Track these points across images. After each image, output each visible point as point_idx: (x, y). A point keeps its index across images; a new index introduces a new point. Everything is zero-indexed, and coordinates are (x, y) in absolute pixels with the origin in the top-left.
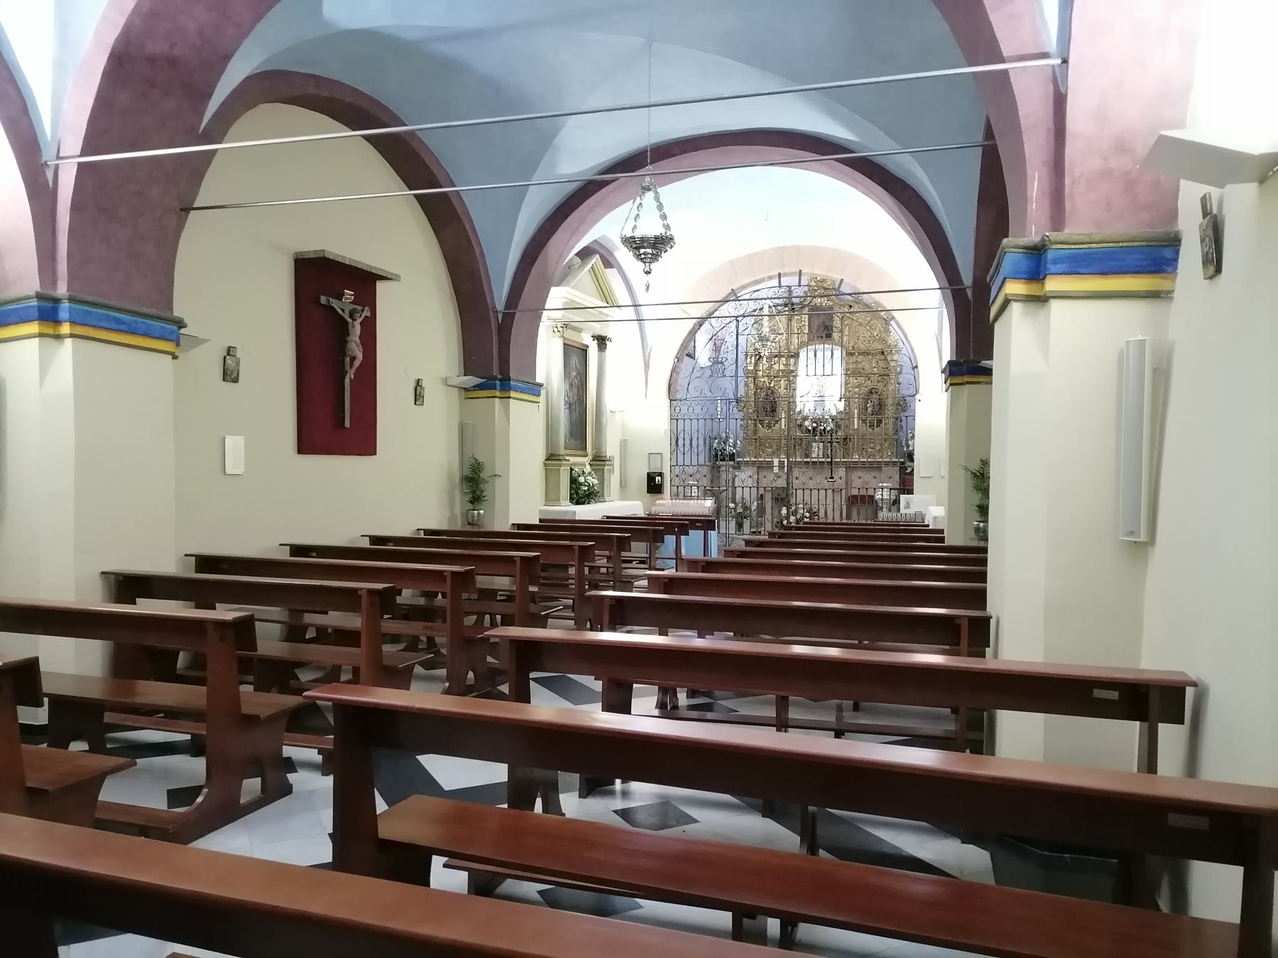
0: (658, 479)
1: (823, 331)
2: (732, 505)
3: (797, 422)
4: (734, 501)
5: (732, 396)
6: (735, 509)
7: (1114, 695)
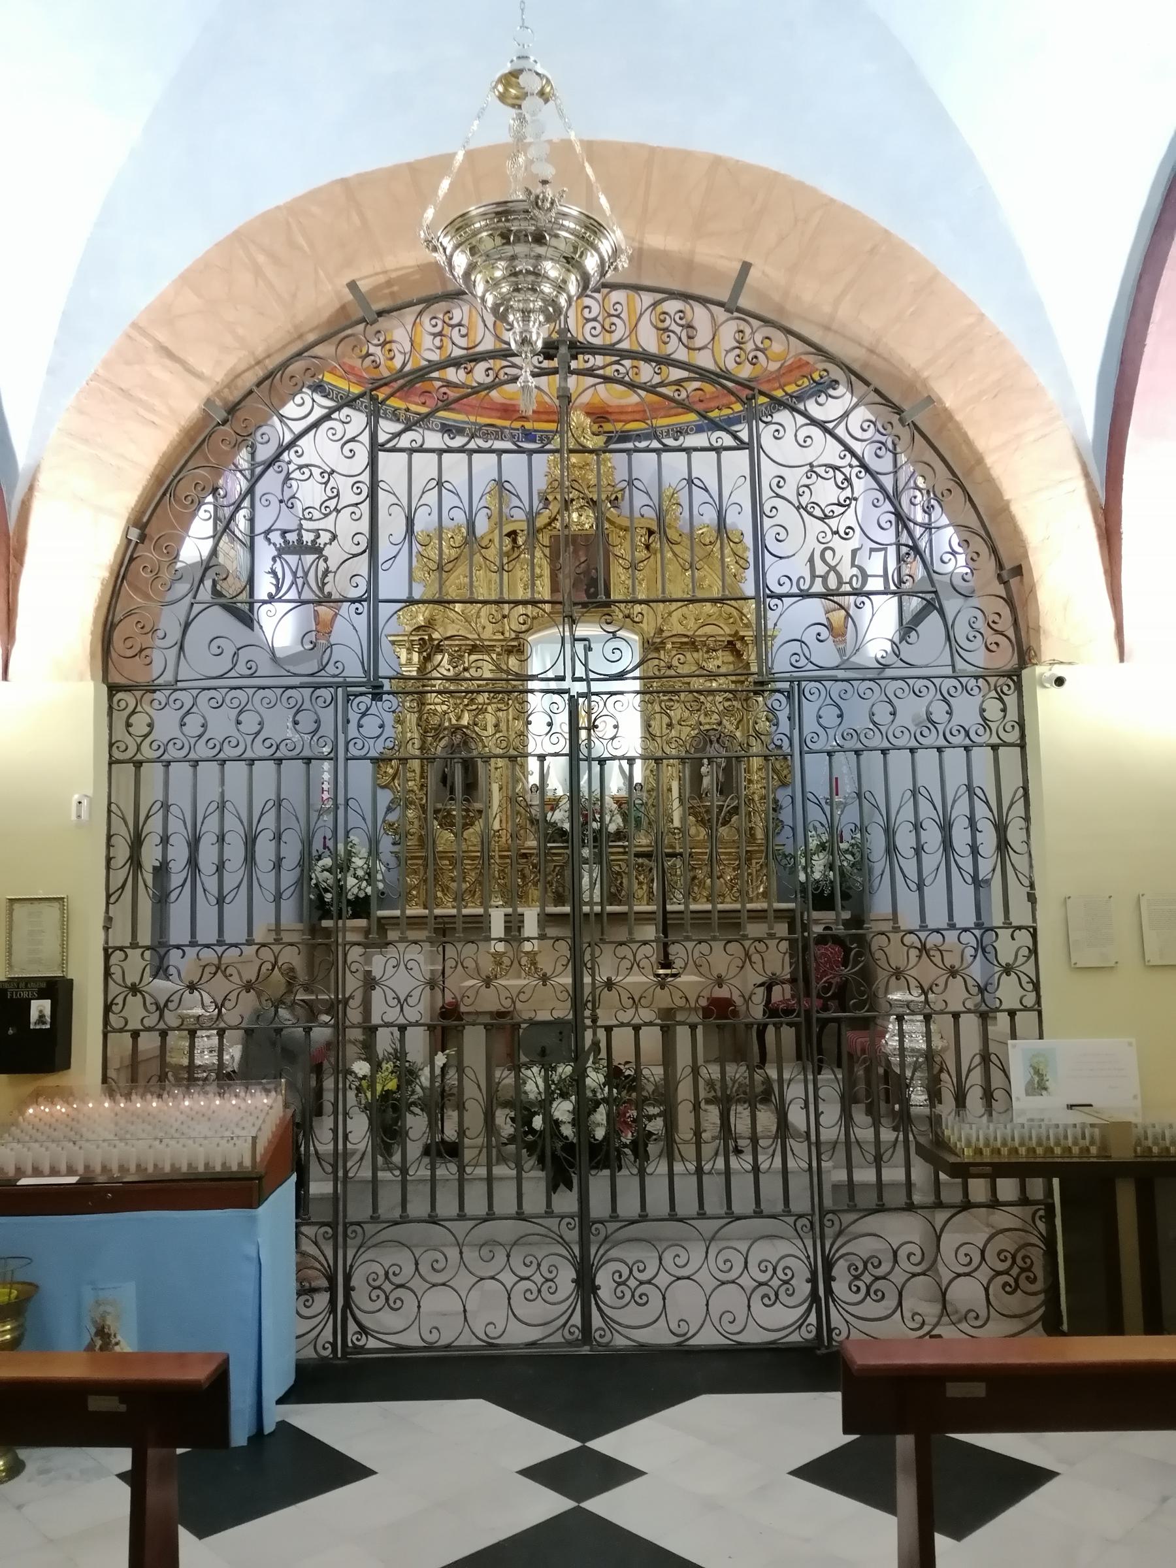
0: (40, 1008)
1: (586, 593)
2: (361, 1068)
3: (530, 811)
4: (368, 1050)
5: (354, 671)
6: (372, 1080)
7: (978, 1390)
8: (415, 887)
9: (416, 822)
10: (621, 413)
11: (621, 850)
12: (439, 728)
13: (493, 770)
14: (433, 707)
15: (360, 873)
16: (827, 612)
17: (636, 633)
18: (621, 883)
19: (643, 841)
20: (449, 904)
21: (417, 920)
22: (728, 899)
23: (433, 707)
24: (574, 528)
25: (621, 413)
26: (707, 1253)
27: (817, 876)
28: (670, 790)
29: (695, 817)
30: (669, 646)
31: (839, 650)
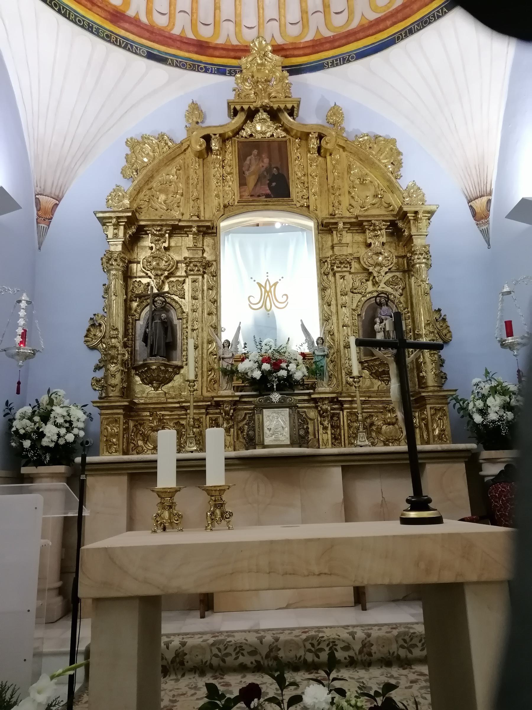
8: (116, 435)
10: (295, 49)
11: (306, 398)
14: (138, 280)
15: (60, 420)
16: (469, 202)
17: (310, 218)
18: (308, 428)
19: (324, 389)
23: (138, 280)
24: (259, 136)
25: (295, 49)
27: (493, 416)
29: (369, 370)
31: (482, 231)
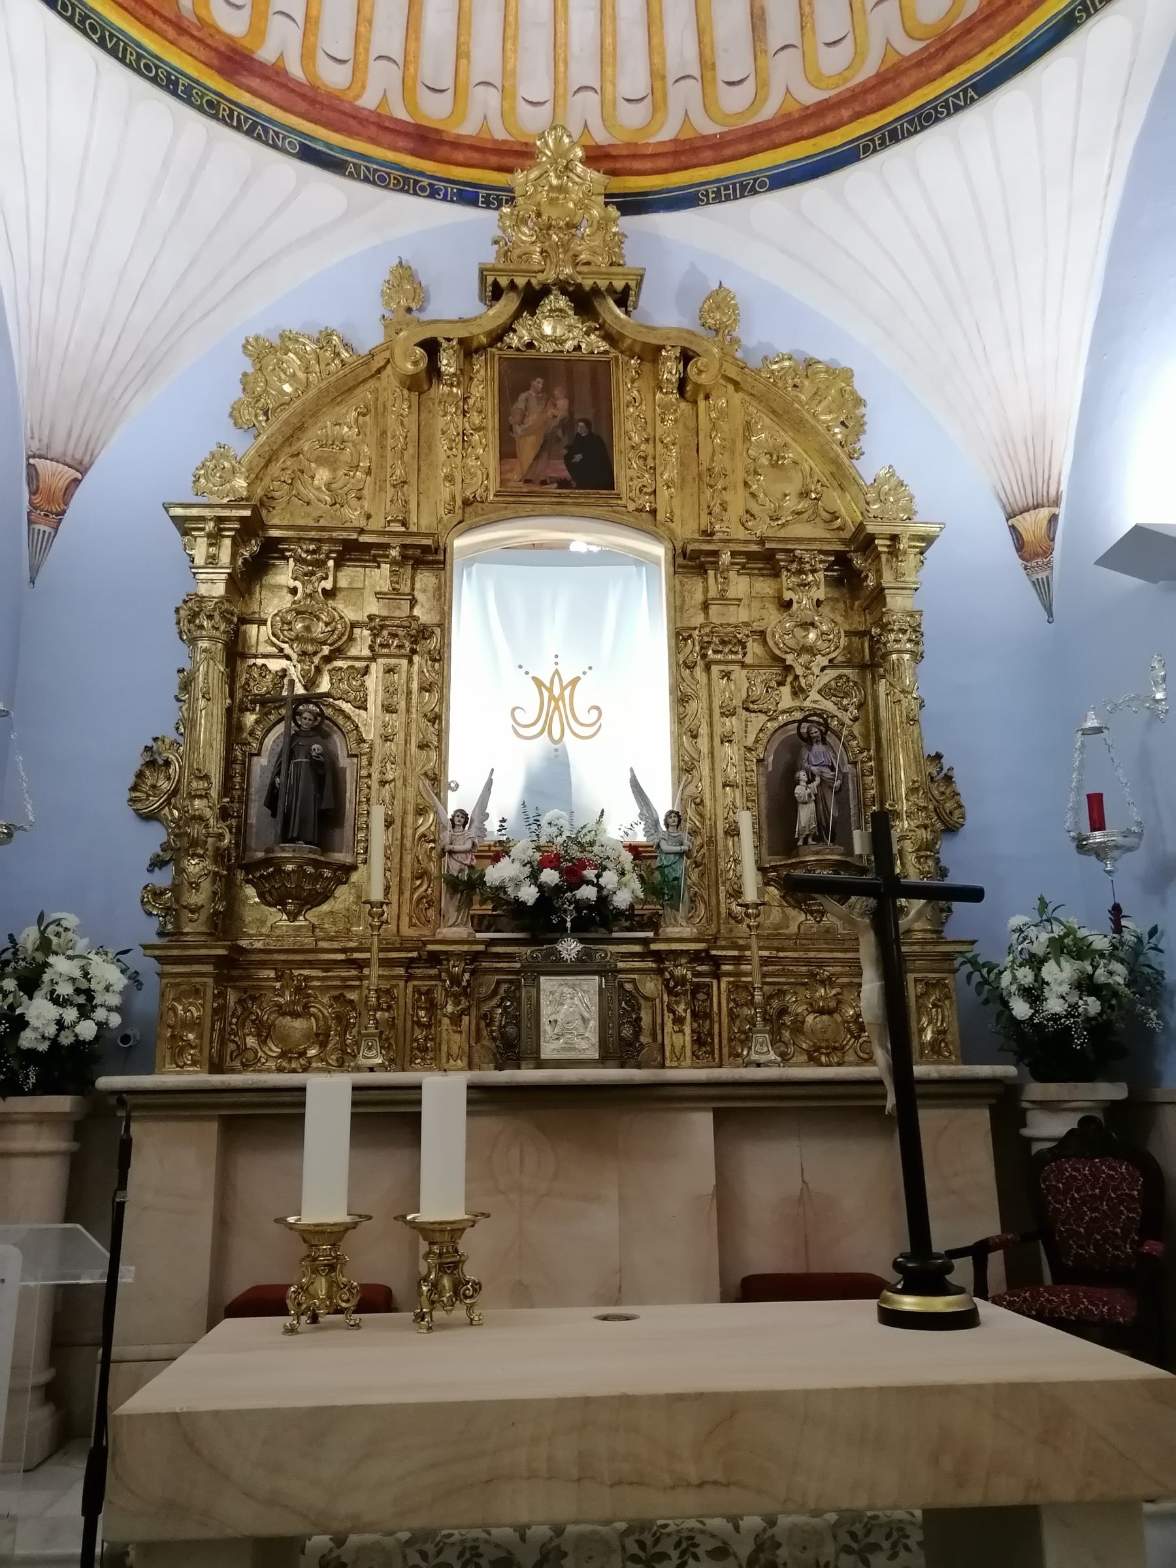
9: (206, 885)
10: (634, 157)
11: (637, 948)
12: (266, 703)
13: (374, 783)
14: (260, 662)
15: (65, 989)
19: (680, 930)
20: (272, 1064)
21: (203, 1099)
22: (850, 1057)
23: (260, 662)
24: (548, 348)
25: (634, 157)
26: (95, 94)
27: (1054, 1005)
28: (733, 831)
30: (726, 558)
